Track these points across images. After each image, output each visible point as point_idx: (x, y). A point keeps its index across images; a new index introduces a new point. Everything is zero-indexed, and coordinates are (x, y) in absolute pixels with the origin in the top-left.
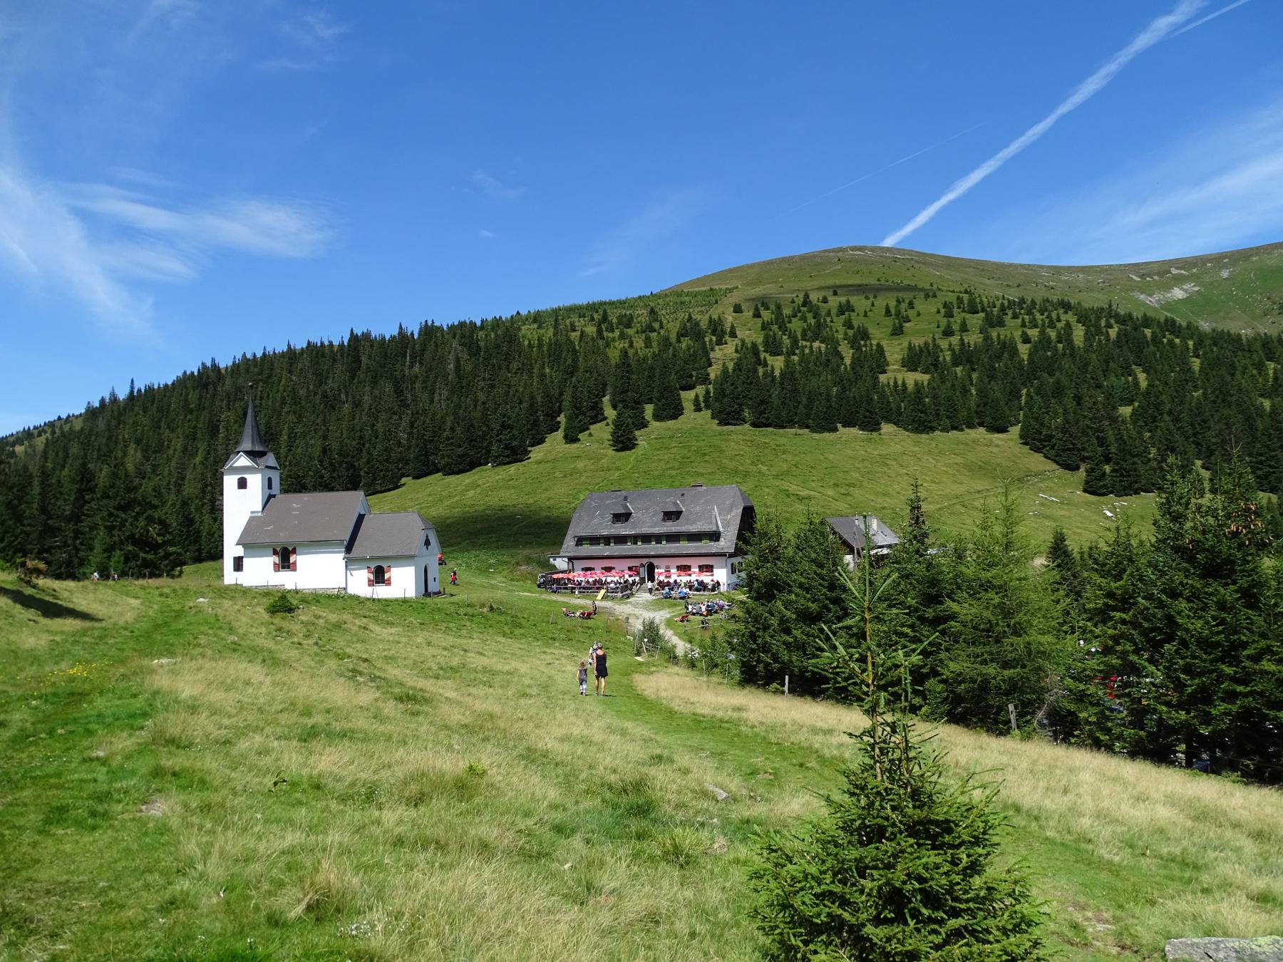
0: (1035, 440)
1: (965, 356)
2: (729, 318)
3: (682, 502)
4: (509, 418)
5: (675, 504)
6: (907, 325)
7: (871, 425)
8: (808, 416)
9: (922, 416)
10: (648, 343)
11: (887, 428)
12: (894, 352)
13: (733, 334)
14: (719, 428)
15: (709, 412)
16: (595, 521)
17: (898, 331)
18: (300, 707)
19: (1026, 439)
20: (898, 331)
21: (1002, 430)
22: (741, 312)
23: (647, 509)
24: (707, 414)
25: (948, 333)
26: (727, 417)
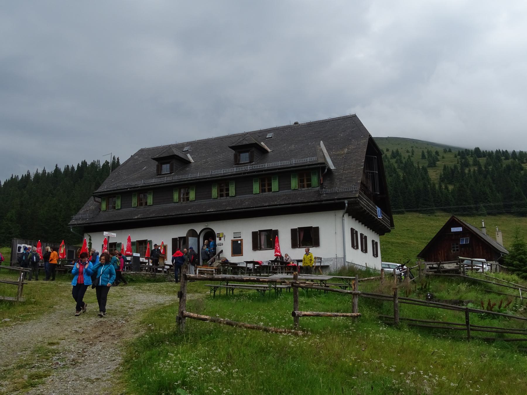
6: (437, 163)
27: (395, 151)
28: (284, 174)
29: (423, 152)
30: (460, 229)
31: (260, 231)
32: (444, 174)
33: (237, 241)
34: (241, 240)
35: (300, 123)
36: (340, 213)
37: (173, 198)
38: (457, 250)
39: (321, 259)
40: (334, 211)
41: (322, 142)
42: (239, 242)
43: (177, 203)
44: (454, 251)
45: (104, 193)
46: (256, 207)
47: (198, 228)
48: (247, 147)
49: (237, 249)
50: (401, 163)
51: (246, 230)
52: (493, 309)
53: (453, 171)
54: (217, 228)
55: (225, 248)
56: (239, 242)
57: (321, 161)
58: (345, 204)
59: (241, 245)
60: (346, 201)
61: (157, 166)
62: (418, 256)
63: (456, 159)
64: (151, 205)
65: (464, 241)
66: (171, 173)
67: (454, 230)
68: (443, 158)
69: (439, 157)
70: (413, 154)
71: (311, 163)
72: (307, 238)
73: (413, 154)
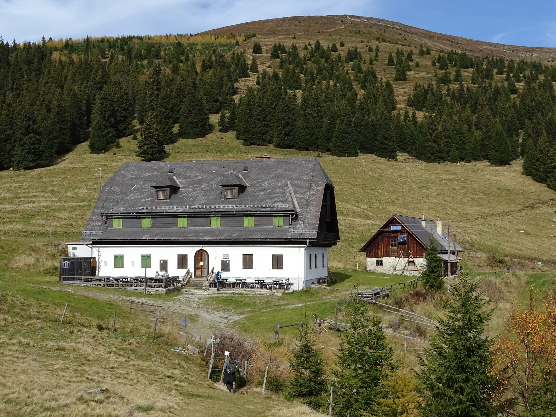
0: (537, 171)
1: (461, 97)
2: (250, 57)
3: (246, 175)
4: (35, 122)
5: (237, 177)
6: (408, 73)
7: (388, 153)
8: (328, 140)
9: (433, 148)
10: (175, 70)
11: (402, 156)
12: (402, 92)
13: (254, 69)
14: (243, 147)
15: (235, 133)
16: (132, 196)
17: (402, 77)
18: (380, 343)
19: (528, 171)
20: (402, 77)
21: (504, 162)
22: (261, 53)
23: (199, 183)
24: (231, 135)
25: (445, 80)
26: (251, 138)
27: (352, 49)
29: (391, 55)
30: (399, 228)
32: (414, 96)
33: (226, 261)
34: (229, 261)
38: (395, 246)
42: (228, 262)
44: (392, 246)
49: (226, 266)
50: (360, 71)
51: (236, 254)
52: (263, 370)
53: (426, 92)
54: (211, 250)
55: (215, 264)
56: (228, 262)
57: (291, 208)
59: (229, 264)
62: (360, 250)
63: (434, 68)
65: (402, 238)
67: (394, 228)
68: (417, 65)
69: (411, 63)
70: (377, 55)
73: (377, 55)
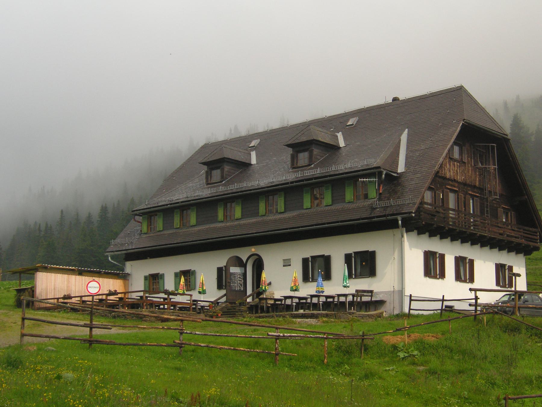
28: (352, 178)
31: (313, 258)
35: (401, 98)
36: (397, 232)
37: (217, 216)
39: (371, 292)
40: (391, 230)
41: (406, 131)
43: (222, 221)
45: (148, 210)
46: (316, 225)
47: (244, 253)
48: (305, 142)
58: (397, 221)
60: (399, 218)
61: (207, 172)
64: (193, 228)
66: (309, 165)
71: (347, 171)
72: (364, 264)
